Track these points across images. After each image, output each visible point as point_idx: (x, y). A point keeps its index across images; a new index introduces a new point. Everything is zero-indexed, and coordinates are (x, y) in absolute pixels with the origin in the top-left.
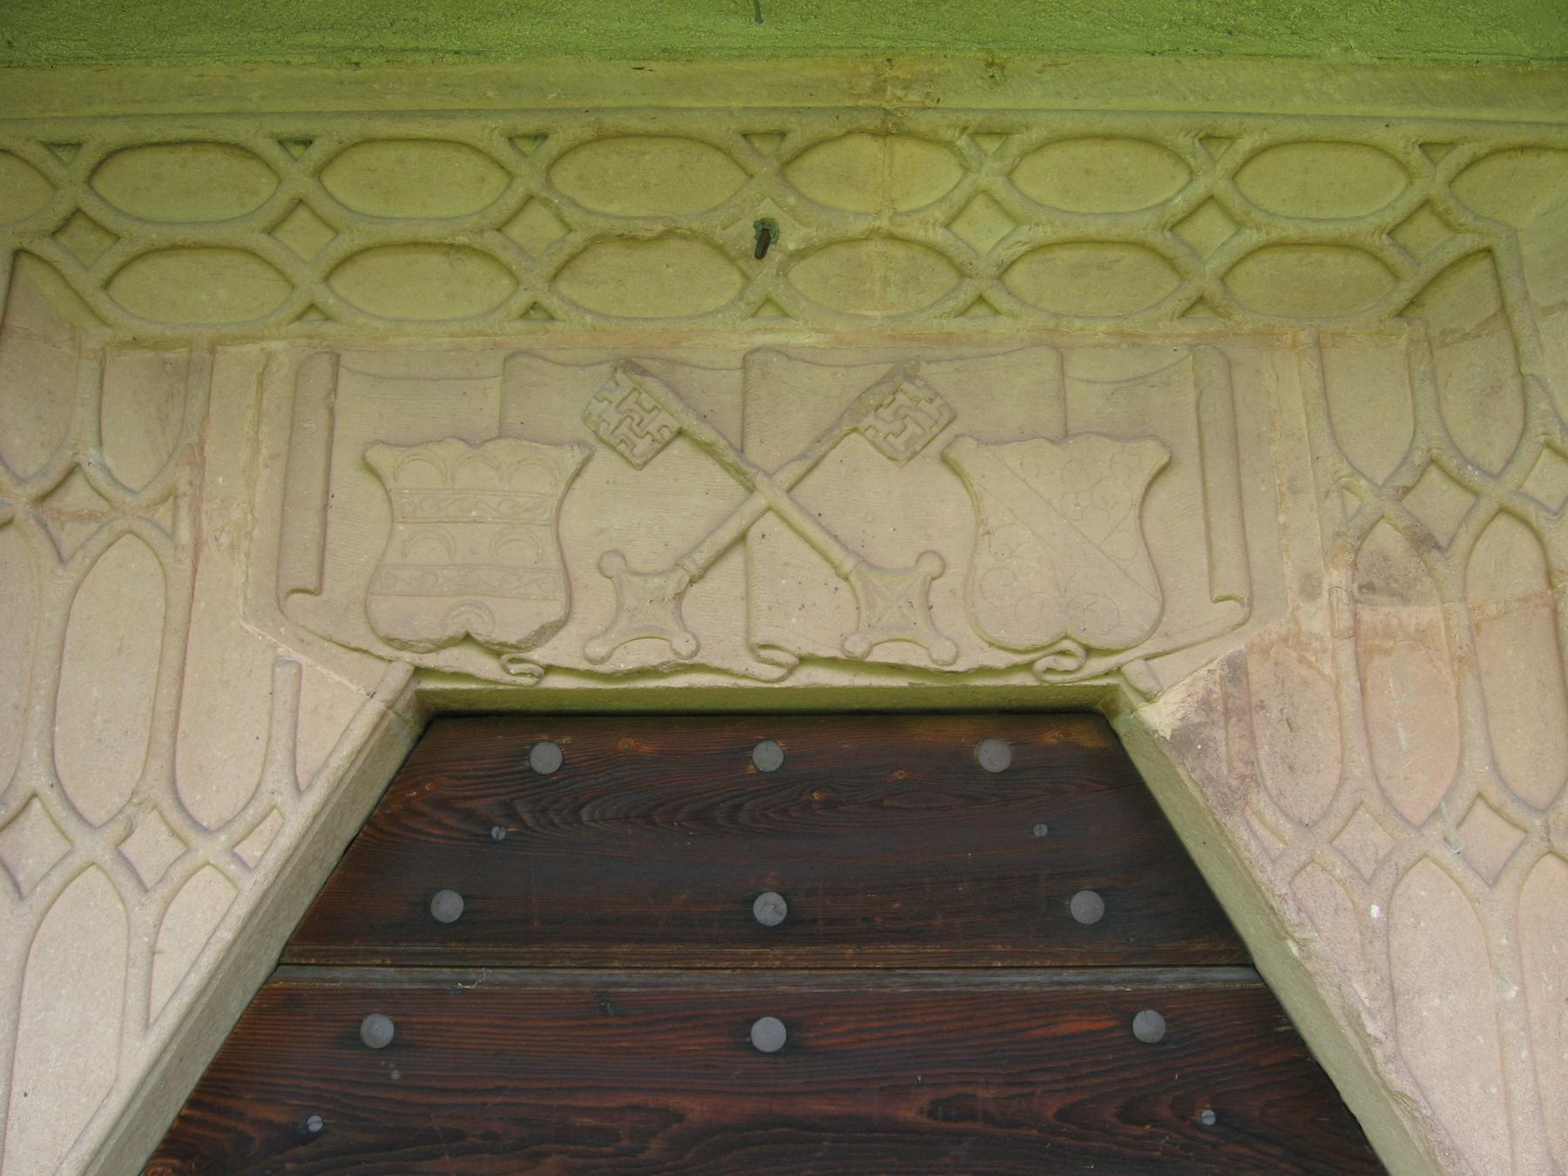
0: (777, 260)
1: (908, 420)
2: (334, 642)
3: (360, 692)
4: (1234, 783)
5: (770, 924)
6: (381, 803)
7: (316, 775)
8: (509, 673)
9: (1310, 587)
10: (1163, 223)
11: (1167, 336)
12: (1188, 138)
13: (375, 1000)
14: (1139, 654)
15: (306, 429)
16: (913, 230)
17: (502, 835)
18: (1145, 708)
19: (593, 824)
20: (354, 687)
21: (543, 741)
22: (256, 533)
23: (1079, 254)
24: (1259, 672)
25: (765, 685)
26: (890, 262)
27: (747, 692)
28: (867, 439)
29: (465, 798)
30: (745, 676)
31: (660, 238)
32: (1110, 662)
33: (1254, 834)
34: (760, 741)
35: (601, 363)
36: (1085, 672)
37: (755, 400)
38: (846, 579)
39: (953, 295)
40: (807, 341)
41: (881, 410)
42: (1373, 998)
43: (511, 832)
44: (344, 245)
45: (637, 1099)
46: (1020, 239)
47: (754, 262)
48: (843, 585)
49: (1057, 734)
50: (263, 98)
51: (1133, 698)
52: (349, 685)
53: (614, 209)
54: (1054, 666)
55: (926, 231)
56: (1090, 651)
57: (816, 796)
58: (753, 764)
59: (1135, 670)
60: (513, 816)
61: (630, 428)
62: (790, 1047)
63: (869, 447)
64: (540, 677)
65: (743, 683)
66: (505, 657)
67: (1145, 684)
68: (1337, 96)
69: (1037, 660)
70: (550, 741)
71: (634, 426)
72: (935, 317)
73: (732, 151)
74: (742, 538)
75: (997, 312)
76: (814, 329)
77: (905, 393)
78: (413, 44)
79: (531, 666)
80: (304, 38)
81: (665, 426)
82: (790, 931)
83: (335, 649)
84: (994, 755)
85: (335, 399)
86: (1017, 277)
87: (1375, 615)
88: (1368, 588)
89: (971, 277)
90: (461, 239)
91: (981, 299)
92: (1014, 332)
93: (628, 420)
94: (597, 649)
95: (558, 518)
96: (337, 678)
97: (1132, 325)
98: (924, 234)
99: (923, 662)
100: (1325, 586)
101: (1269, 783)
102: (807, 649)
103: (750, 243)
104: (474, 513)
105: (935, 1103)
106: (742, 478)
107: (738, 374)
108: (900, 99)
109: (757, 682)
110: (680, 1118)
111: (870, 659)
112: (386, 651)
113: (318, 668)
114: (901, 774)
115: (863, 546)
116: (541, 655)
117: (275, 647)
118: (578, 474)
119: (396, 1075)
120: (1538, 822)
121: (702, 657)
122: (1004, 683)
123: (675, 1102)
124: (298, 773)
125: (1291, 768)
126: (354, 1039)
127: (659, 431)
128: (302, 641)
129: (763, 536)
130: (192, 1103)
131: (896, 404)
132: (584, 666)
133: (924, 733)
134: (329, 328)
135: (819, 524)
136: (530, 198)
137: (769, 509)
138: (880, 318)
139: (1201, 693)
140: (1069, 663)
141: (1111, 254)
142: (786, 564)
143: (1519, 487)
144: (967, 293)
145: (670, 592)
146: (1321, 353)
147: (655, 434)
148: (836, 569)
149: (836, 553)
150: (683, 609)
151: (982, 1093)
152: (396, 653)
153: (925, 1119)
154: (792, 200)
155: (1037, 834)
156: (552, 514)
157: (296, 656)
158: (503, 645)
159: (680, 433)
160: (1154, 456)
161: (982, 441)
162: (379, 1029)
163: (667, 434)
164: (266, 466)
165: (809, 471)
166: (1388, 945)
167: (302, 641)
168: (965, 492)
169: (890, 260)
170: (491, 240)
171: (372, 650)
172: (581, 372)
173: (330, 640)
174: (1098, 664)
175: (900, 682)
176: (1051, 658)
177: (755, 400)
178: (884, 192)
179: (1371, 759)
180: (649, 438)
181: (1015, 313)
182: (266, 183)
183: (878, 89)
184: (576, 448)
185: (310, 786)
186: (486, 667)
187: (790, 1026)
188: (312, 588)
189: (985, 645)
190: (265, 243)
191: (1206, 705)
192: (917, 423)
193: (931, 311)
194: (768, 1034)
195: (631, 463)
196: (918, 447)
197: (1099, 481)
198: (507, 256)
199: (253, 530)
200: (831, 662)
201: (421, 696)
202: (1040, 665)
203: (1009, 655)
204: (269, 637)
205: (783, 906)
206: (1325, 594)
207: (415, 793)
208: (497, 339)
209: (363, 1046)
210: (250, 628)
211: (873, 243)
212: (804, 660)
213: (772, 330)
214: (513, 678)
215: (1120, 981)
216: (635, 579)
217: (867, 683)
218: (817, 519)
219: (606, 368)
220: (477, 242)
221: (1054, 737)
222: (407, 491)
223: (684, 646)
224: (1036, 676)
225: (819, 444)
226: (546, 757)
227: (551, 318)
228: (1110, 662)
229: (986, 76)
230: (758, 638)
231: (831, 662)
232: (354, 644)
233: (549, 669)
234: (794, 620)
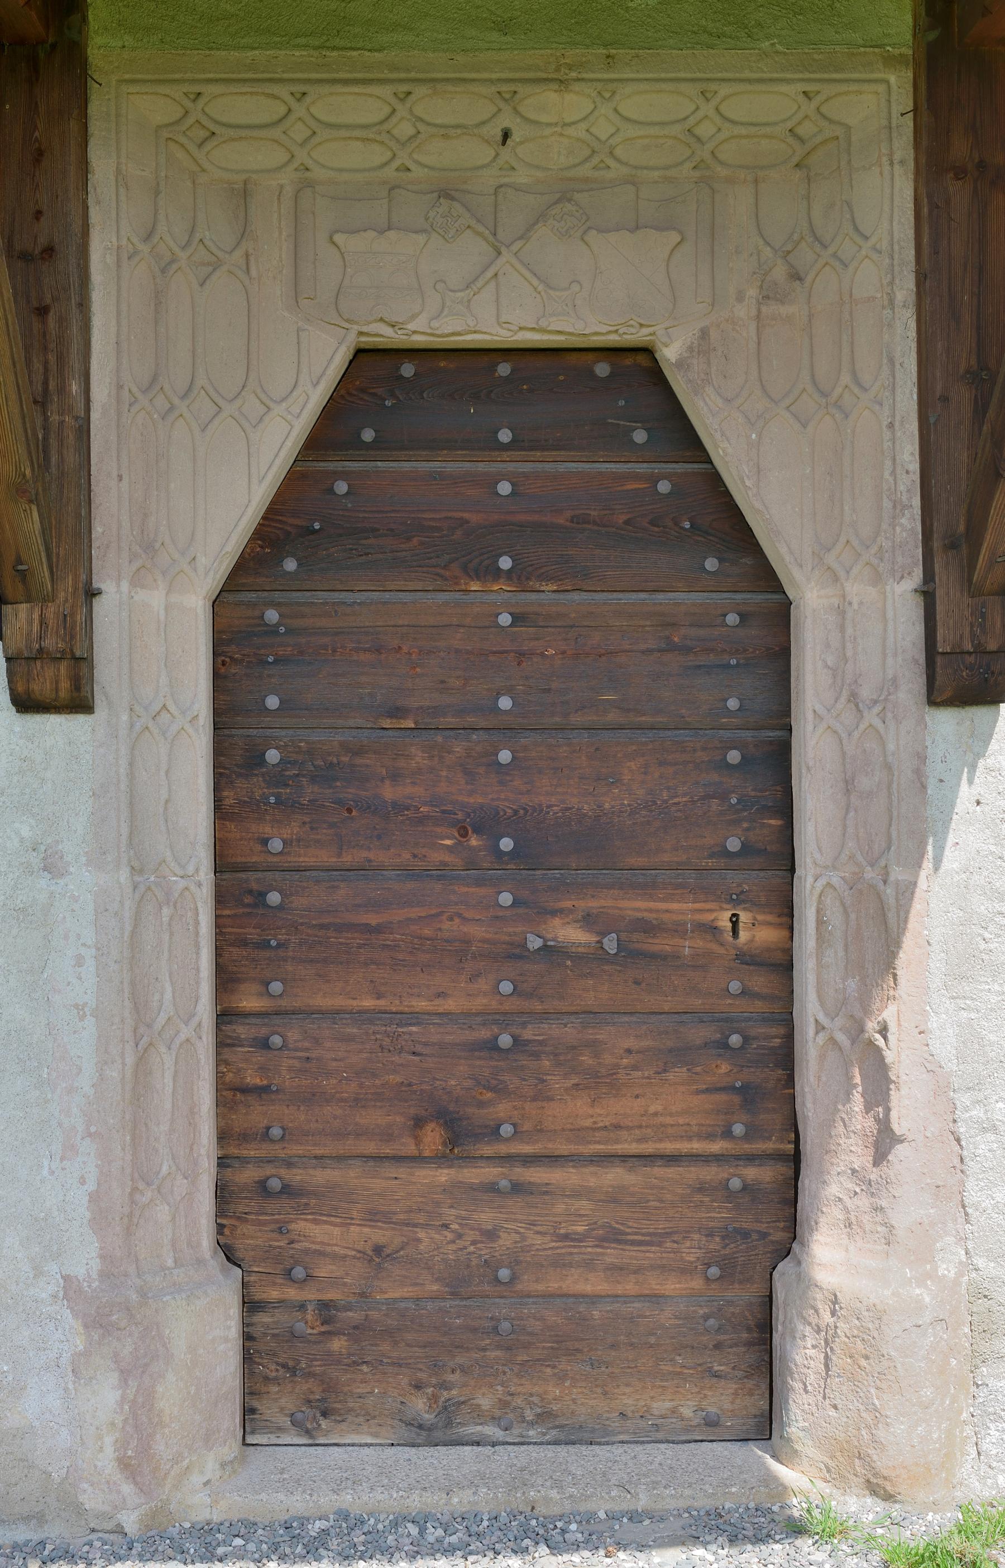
4: (699, 382)
5: (505, 442)
9: (740, 297)
13: (344, 475)
17: (390, 404)
22: (284, 271)
24: (714, 334)
27: (497, 341)
29: (373, 388)
32: (651, 330)
33: (706, 404)
35: (432, 192)
36: (640, 334)
38: (539, 293)
42: (750, 471)
45: (450, 514)
47: (501, 147)
48: (538, 296)
50: (283, 72)
51: (660, 344)
56: (641, 325)
57: (525, 387)
60: (393, 395)
62: (513, 493)
66: (397, 327)
67: (664, 339)
68: (765, 69)
78: (349, 45)
80: (299, 41)
82: (513, 445)
84: (602, 369)
87: (769, 309)
88: (767, 297)
100: (747, 297)
101: (715, 382)
103: (499, 138)
105: (573, 517)
107: (493, 197)
108: (567, 75)
110: (468, 522)
111: (549, 329)
112: (346, 325)
116: (411, 326)
117: (297, 323)
119: (350, 505)
120: (824, 401)
123: (466, 515)
125: (725, 377)
126: (331, 491)
130: (263, 518)
132: (429, 331)
133: (573, 359)
135: (529, 269)
139: (689, 343)
143: (835, 253)
146: (757, 185)
148: (535, 289)
149: (535, 282)
151: (593, 513)
152: (350, 326)
153: (568, 524)
158: (396, 322)
159: (469, 227)
160: (675, 237)
161: (600, 231)
162: (341, 487)
166: (759, 450)
173: (322, 320)
174: (645, 331)
175: (562, 338)
179: (760, 372)
183: (557, 70)
186: (388, 331)
187: (513, 484)
191: (690, 349)
194: (505, 488)
200: (533, 329)
201: (359, 342)
202: (621, 331)
205: (510, 435)
206: (747, 300)
209: (335, 494)
210: (286, 314)
215: (657, 468)
216: (450, 293)
218: (527, 266)
219: (436, 195)
223: (471, 323)
224: (620, 335)
226: (408, 370)
228: (651, 330)
229: (606, 63)
231: (533, 329)
233: (414, 332)
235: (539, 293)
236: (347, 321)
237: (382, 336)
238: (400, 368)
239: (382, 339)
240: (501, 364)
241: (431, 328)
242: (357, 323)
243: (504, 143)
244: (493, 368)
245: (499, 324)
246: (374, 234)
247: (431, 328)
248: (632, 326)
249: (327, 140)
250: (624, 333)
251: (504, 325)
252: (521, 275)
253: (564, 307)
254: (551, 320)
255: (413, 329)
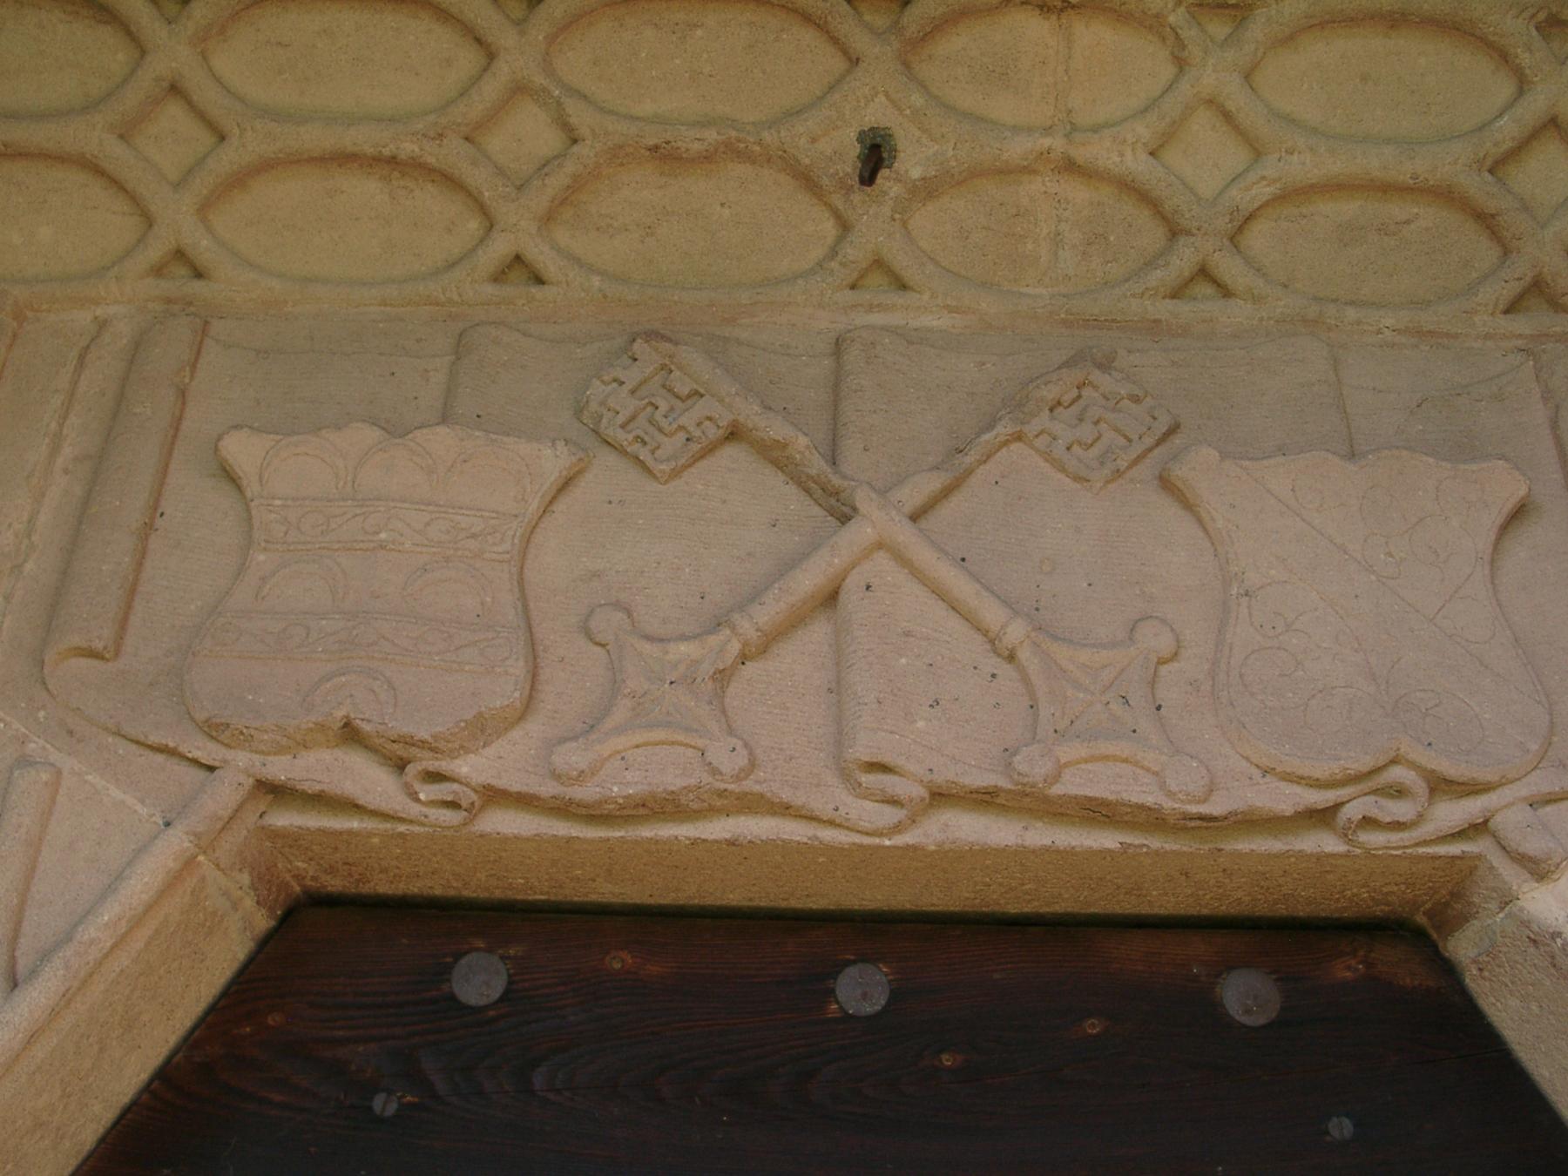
0: (892, 195)
1: (1103, 426)
2: (124, 737)
3: (154, 819)
6: (193, 1041)
7: (45, 956)
8: (418, 800)
10: (1481, 155)
11: (1487, 337)
12: (1520, 20)
14: (1524, 792)
15: (135, 414)
16: (1100, 152)
17: (392, 1108)
18: (1535, 894)
19: (551, 1096)
20: (143, 811)
21: (477, 949)
23: (1348, 208)
25: (867, 840)
26: (1065, 210)
28: (1037, 450)
30: (831, 823)
31: (708, 158)
34: (848, 963)
36: (1427, 830)
37: (856, 391)
38: (1011, 657)
39: (1161, 262)
40: (935, 323)
41: (1060, 409)
43: (410, 1104)
44: (229, 158)
46: (1265, 173)
48: (1005, 670)
49: (1353, 962)
51: (1508, 872)
52: (139, 807)
53: (647, 108)
54: (1374, 813)
55: (1122, 155)
56: (1441, 786)
57: (947, 1060)
58: (837, 1002)
59: (1513, 821)
61: (651, 422)
63: (1042, 463)
64: (473, 812)
65: (828, 835)
69: (1343, 804)
70: (490, 950)
71: (658, 415)
72: (1133, 296)
73: (829, 18)
74: (830, 598)
75: (1226, 292)
76: (946, 307)
77: (1095, 388)
79: (455, 786)
81: (709, 419)
83: (123, 747)
85: (192, 377)
86: (1259, 238)
89: (1189, 233)
90: (408, 148)
91: (1204, 273)
92: (1255, 322)
93: (649, 409)
94: (573, 757)
95: (524, 554)
96: (116, 793)
97: (1435, 319)
98: (1118, 159)
99: (1145, 794)
102: (946, 774)
103: (850, 162)
104: (383, 536)
106: (833, 501)
107: (827, 362)
109: (852, 834)
113: (89, 778)
114: (1093, 1024)
115: (1037, 609)
116: (472, 767)
118: (566, 484)
121: (757, 782)
122: (1286, 848)
124: (18, 953)
127: (699, 425)
128: (71, 733)
129: (868, 587)
131: (1082, 402)
132: (548, 789)
134: (198, 287)
136: (519, 89)
137: (880, 545)
138: (1048, 297)
140: (1401, 810)
141: (1396, 210)
142: (908, 634)
144: (1183, 260)
145: (707, 669)
147: (691, 429)
148: (992, 641)
150: (727, 700)
154: (917, 99)
155: (1335, 1133)
156: (513, 544)
157: (55, 756)
158: (410, 742)
159: (734, 434)
163: (713, 433)
164: (66, 471)
165: (946, 492)
167: (71, 733)
168: (1201, 534)
169: (1063, 206)
170: (452, 154)
171: (183, 749)
172: (578, 350)
173: (118, 734)
174: (1452, 813)
176: (1372, 798)
177: (856, 391)
178: (1057, 99)
180: (682, 436)
181: (1256, 292)
182: (118, 56)
184: (560, 444)
185: (34, 973)
188: (98, 645)
189: (1256, 773)
190: (114, 153)
192: (1117, 430)
193: (1127, 285)
195: (648, 471)
196: (1123, 464)
197: (1421, 520)
198: (478, 177)
199: (25, 561)
200: (985, 800)
202: (1353, 811)
203: (1298, 789)
204: (16, 725)
207: (248, 1029)
208: (453, 310)
211: (1039, 179)
212: (941, 797)
213: (881, 308)
214: (425, 810)
216: (647, 647)
217: (1047, 842)
220: (433, 155)
221: (1349, 968)
222: (278, 502)
223: (727, 759)
224: (1345, 835)
225: (960, 455)
227: (539, 280)
230: (862, 750)
231: (985, 800)
232: (154, 739)
233: (494, 796)
234: (921, 724)
235: (1011, 657)
236: (213, 730)
237: (352, 807)
238: (448, 969)
239: (355, 824)
240: (852, 971)
241: (556, 776)
242: (243, 740)
243: (868, 177)
244: (820, 981)
245: (845, 775)
246: (372, 434)
247: (556, 776)
248: (1399, 792)
249: (266, 166)
250: (1368, 822)
251: (867, 779)
252: (940, 594)
253: (1116, 707)
254: (1066, 752)
255: (479, 779)
